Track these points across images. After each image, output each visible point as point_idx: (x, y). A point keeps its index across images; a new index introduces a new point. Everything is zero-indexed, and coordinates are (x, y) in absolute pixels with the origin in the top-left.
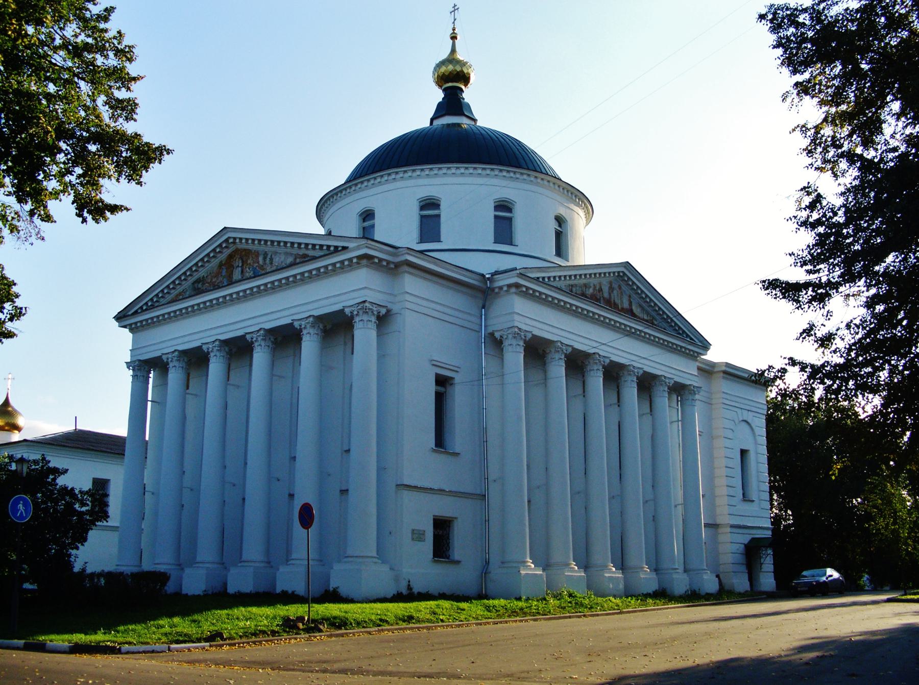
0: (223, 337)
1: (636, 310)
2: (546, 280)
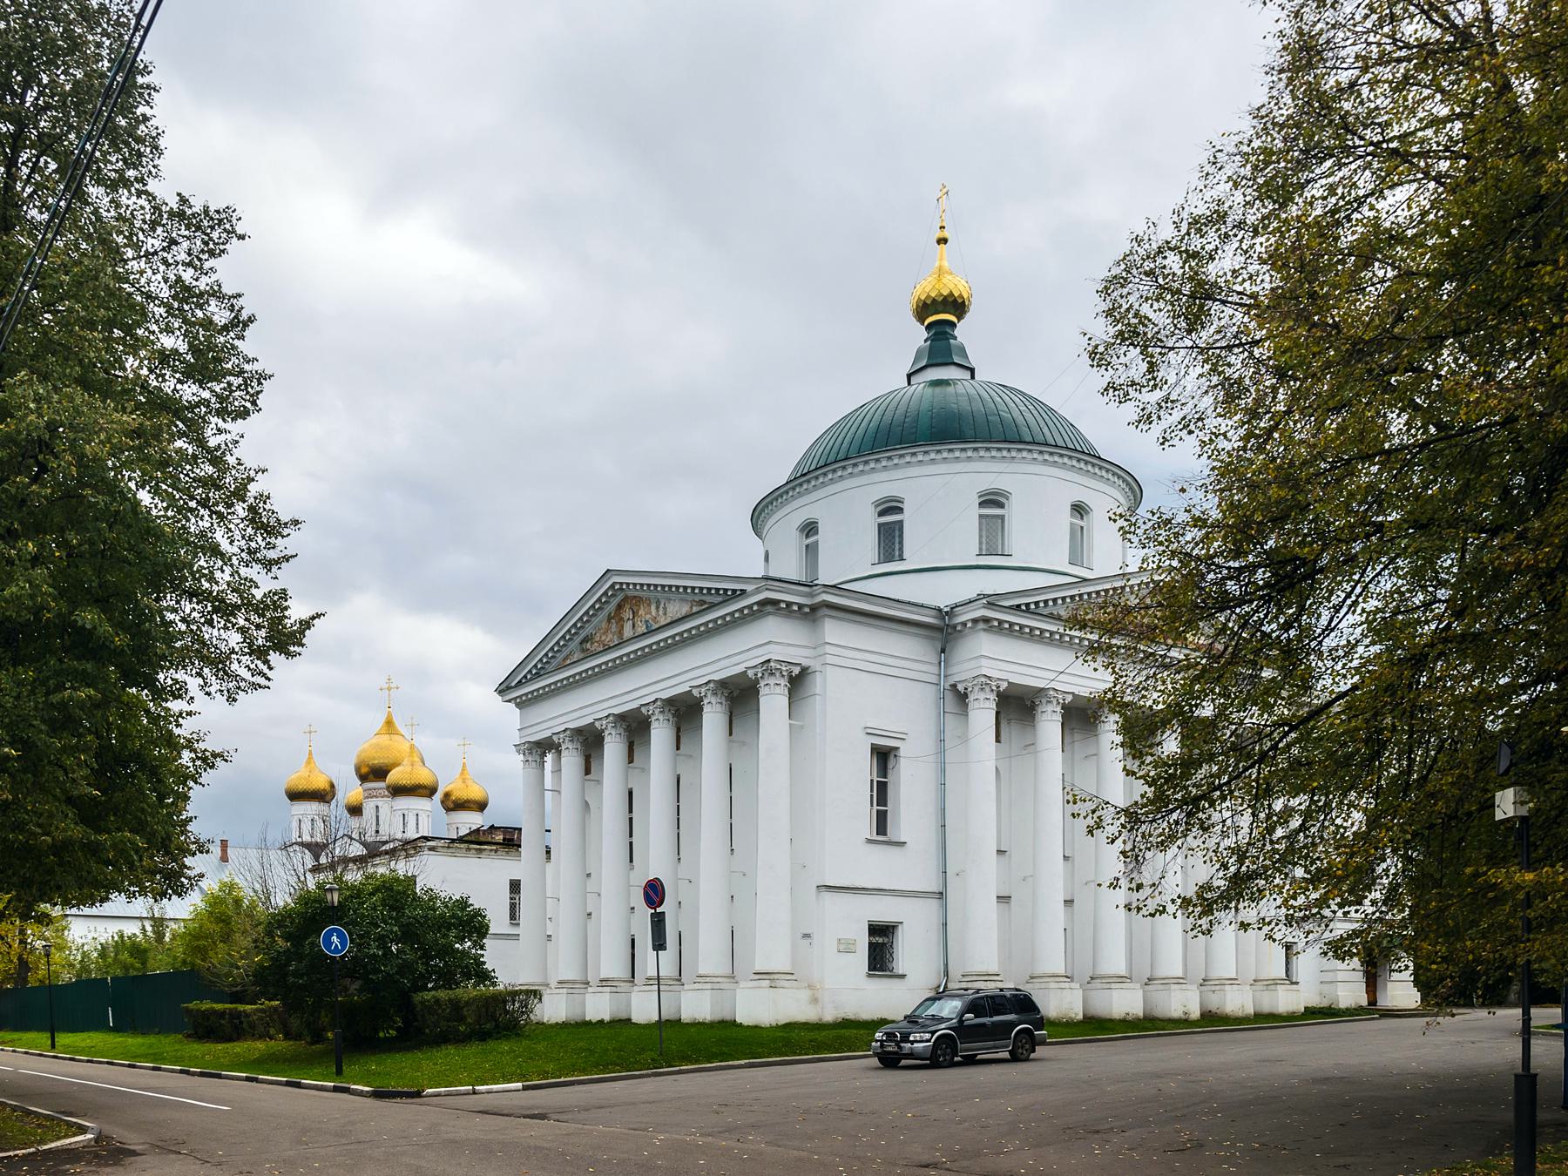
0: (617, 711)
2: (1033, 606)
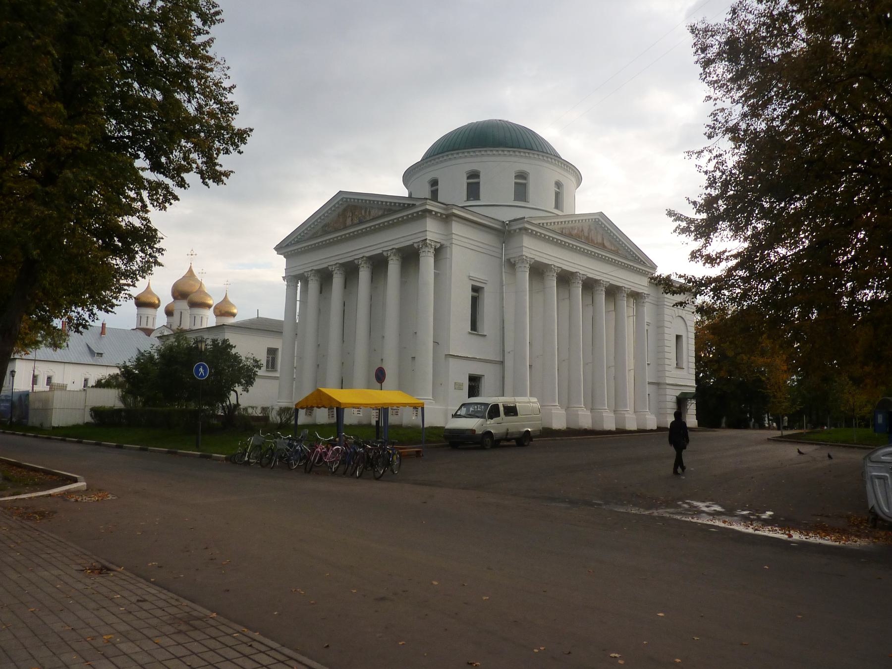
1: (607, 244)
2: (545, 225)
